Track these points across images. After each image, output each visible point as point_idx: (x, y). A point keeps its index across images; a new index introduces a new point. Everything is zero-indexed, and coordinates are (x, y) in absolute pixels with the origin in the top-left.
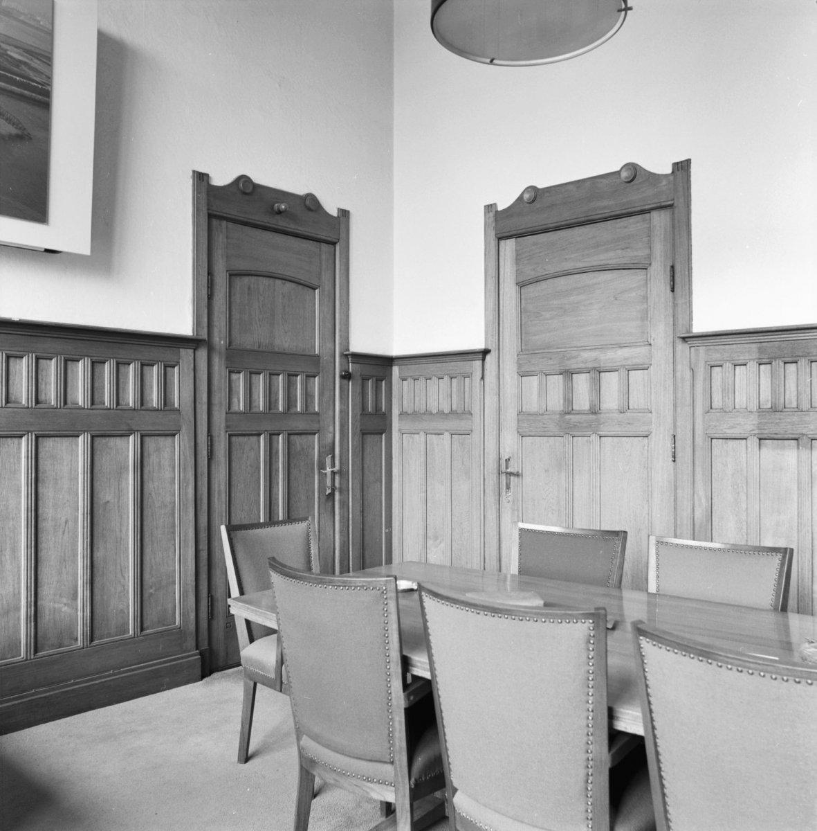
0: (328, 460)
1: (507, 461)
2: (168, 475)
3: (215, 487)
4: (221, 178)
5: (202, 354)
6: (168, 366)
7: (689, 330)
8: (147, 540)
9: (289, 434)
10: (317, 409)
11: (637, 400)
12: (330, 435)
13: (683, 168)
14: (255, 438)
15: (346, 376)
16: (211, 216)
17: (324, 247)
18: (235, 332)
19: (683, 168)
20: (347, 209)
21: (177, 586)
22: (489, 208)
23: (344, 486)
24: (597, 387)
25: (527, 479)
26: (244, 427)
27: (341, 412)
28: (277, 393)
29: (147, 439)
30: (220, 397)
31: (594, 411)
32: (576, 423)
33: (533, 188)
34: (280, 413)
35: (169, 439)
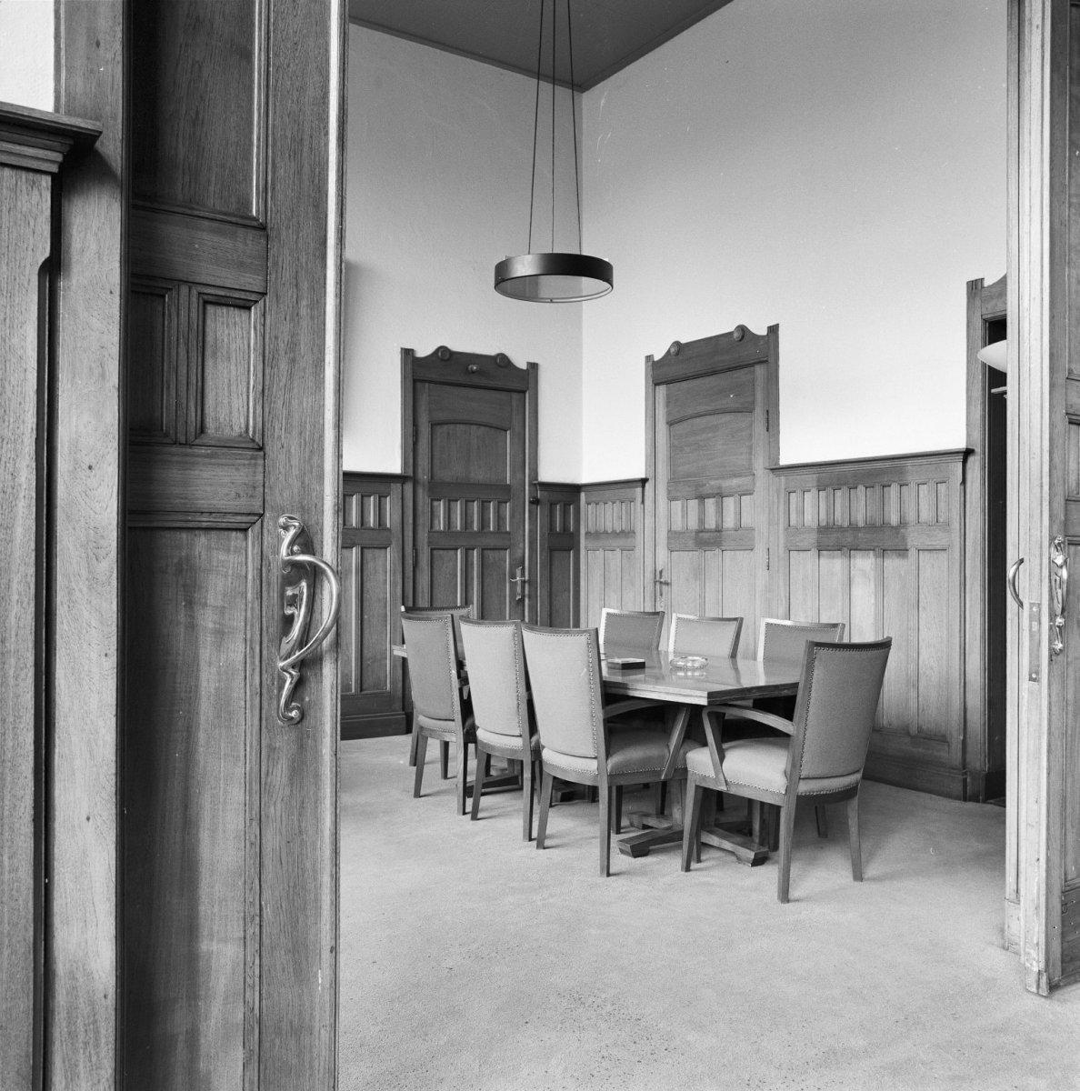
0: (518, 572)
1: (661, 572)
2: (381, 578)
3: (419, 588)
4: (423, 351)
5: (409, 487)
6: (382, 497)
7: (777, 462)
8: (365, 626)
9: (483, 550)
10: (388, 526)
11: (746, 521)
12: (520, 551)
13: (774, 330)
14: (452, 552)
15: (535, 502)
16: (415, 381)
17: (515, 396)
18: (436, 469)
19: (774, 330)
20: (536, 361)
21: (388, 662)
22: (649, 358)
23: (533, 593)
24: (720, 511)
25: (674, 587)
26: (444, 543)
27: (530, 531)
28: (472, 517)
29: (366, 550)
30: (423, 520)
31: (719, 530)
32: (708, 539)
33: (677, 343)
34: (491, 533)
35: (383, 551)
